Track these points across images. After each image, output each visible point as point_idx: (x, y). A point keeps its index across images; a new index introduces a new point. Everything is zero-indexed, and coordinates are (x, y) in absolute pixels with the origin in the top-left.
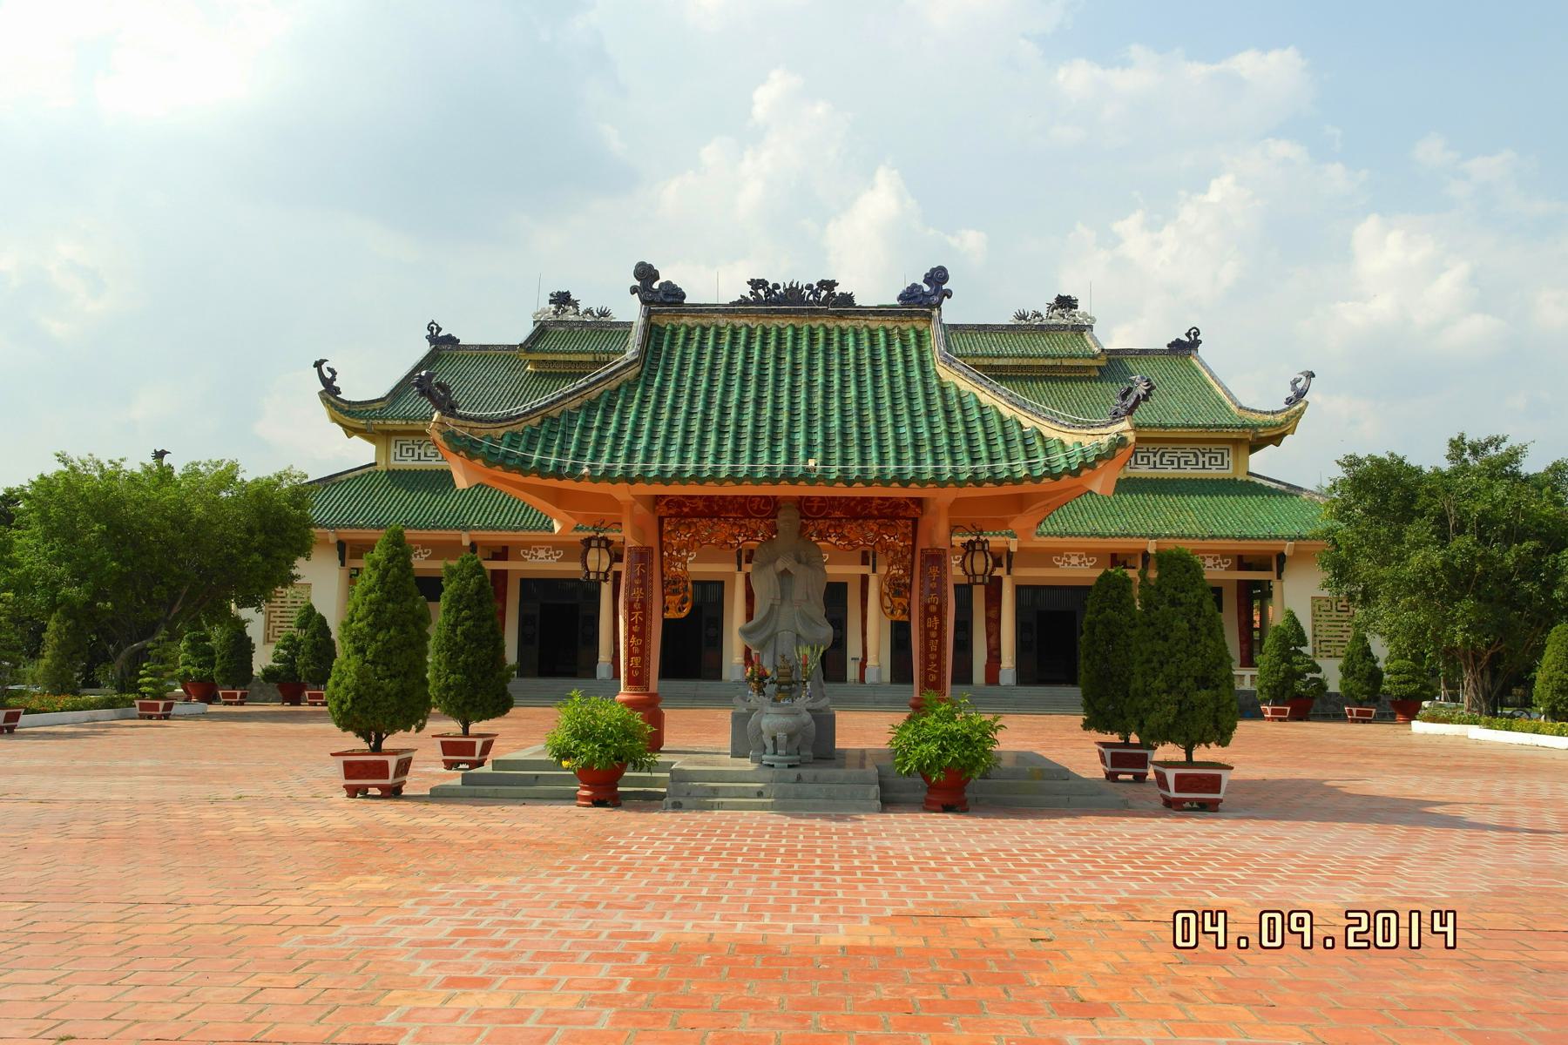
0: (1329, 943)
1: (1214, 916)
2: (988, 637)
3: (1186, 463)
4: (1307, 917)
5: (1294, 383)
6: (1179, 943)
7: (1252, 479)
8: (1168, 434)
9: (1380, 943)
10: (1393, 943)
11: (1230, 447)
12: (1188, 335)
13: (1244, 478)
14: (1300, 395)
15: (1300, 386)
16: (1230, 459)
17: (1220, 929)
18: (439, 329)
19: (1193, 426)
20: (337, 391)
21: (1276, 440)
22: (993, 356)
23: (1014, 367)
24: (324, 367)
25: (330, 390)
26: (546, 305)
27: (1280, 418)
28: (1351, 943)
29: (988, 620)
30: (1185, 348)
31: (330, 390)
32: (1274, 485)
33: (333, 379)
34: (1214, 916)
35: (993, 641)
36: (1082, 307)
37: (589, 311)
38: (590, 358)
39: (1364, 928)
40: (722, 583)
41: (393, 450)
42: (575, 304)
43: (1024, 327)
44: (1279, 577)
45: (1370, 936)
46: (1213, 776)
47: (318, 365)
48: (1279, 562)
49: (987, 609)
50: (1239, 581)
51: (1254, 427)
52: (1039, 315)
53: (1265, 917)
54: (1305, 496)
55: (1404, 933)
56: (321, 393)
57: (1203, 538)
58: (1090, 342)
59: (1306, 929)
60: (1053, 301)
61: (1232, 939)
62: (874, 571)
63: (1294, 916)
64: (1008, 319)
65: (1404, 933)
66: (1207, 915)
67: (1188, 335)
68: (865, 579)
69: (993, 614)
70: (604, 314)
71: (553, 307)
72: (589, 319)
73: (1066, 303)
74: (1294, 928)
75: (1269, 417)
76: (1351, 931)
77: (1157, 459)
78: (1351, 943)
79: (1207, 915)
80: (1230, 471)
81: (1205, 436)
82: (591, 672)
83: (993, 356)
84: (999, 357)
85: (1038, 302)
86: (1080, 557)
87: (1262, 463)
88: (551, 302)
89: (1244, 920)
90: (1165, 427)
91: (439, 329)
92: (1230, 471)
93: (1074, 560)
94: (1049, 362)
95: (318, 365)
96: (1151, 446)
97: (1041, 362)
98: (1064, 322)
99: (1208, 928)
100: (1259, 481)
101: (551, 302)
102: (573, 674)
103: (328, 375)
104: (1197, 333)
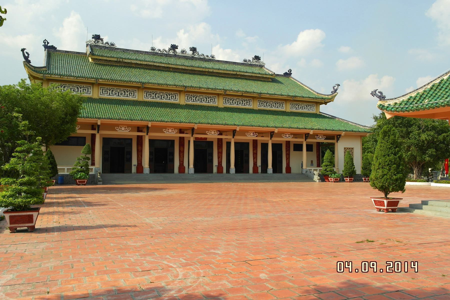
0: (381, 271)
1: (348, 263)
2: (254, 159)
3: (74, 90)
4: (375, 263)
5: (334, 87)
6: (338, 271)
7: (321, 114)
8: (276, 97)
9: (396, 271)
10: (400, 271)
11: (137, 90)
12: (289, 71)
13: (319, 113)
14: (336, 91)
15: (335, 88)
16: (315, 108)
17: (350, 267)
18: (48, 43)
19: (310, 98)
20: (29, 62)
21: (326, 103)
22: (245, 72)
23: (173, 68)
24: (25, 51)
25: (27, 61)
26: (91, 39)
27: (330, 97)
28: (388, 271)
29: (286, 154)
30: (288, 75)
31: (27, 61)
32: (328, 116)
33: (28, 57)
34: (348, 263)
35: (288, 161)
36: (262, 60)
37: (107, 43)
38: (116, 60)
39: (391, 266)
40: (103, 138)
41: (144, 94)
42: (102, 40)
43: (245, 64)
44: (337, 142)
45: (393, 269)
46: (378, 205)
47: (23, 50)
48: (338, 137)
49: (253, 150)
50: (317, 142)
51: (325, 99)
52: (250, 61)
53: (363, 263)
54: (337, 119)
55: (403, 269)
56: (24, 62)
57: (324, 130)
58: (266, 70)
59: (375, 267)
60: (254, 57)
61: (378, 269)
62: (271, 139)
63: (371, 263)
64: (241, 61)
65: (403, 269)
66: (347, 263)
67: (289, 71)
68: (93, 136)
69: (255, 152)
70: (112, 45)
71: (94, 40)
72: (107, 46)
73: (257, 58)
74: (371, 266)
75: (327, 96)
76: (388, 267)
77: (209, 100)
78: (388, 271)
79: (347, 263)
80: (252, 107)
81: (312, 101)
82: (248, 172)
83: (245, 72)
84: (246, 72)
85: (250, 57)
86: (214, 132)
87: (323, 109)
88: (93, 38)
89: (357, 265)
90: (303, 97)
91: (48, 43)
92: (91, 95)
93: (287, 136)
94: (260, 75)
95: (23, 50)
96: (108, 87)
97: (232, 73)
98: (257, 64)
99: (347, 266)
100: (323, 114)
101: (93, 38)
102: (122, 171)
103: (26, 55)
104: (291, 71)
